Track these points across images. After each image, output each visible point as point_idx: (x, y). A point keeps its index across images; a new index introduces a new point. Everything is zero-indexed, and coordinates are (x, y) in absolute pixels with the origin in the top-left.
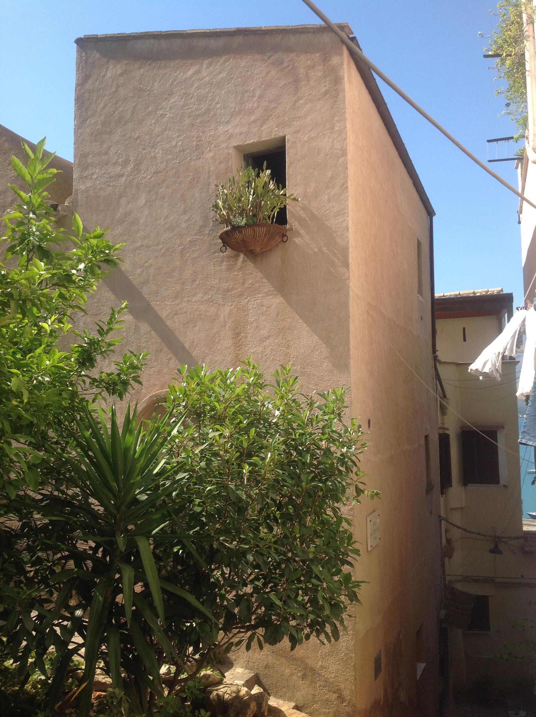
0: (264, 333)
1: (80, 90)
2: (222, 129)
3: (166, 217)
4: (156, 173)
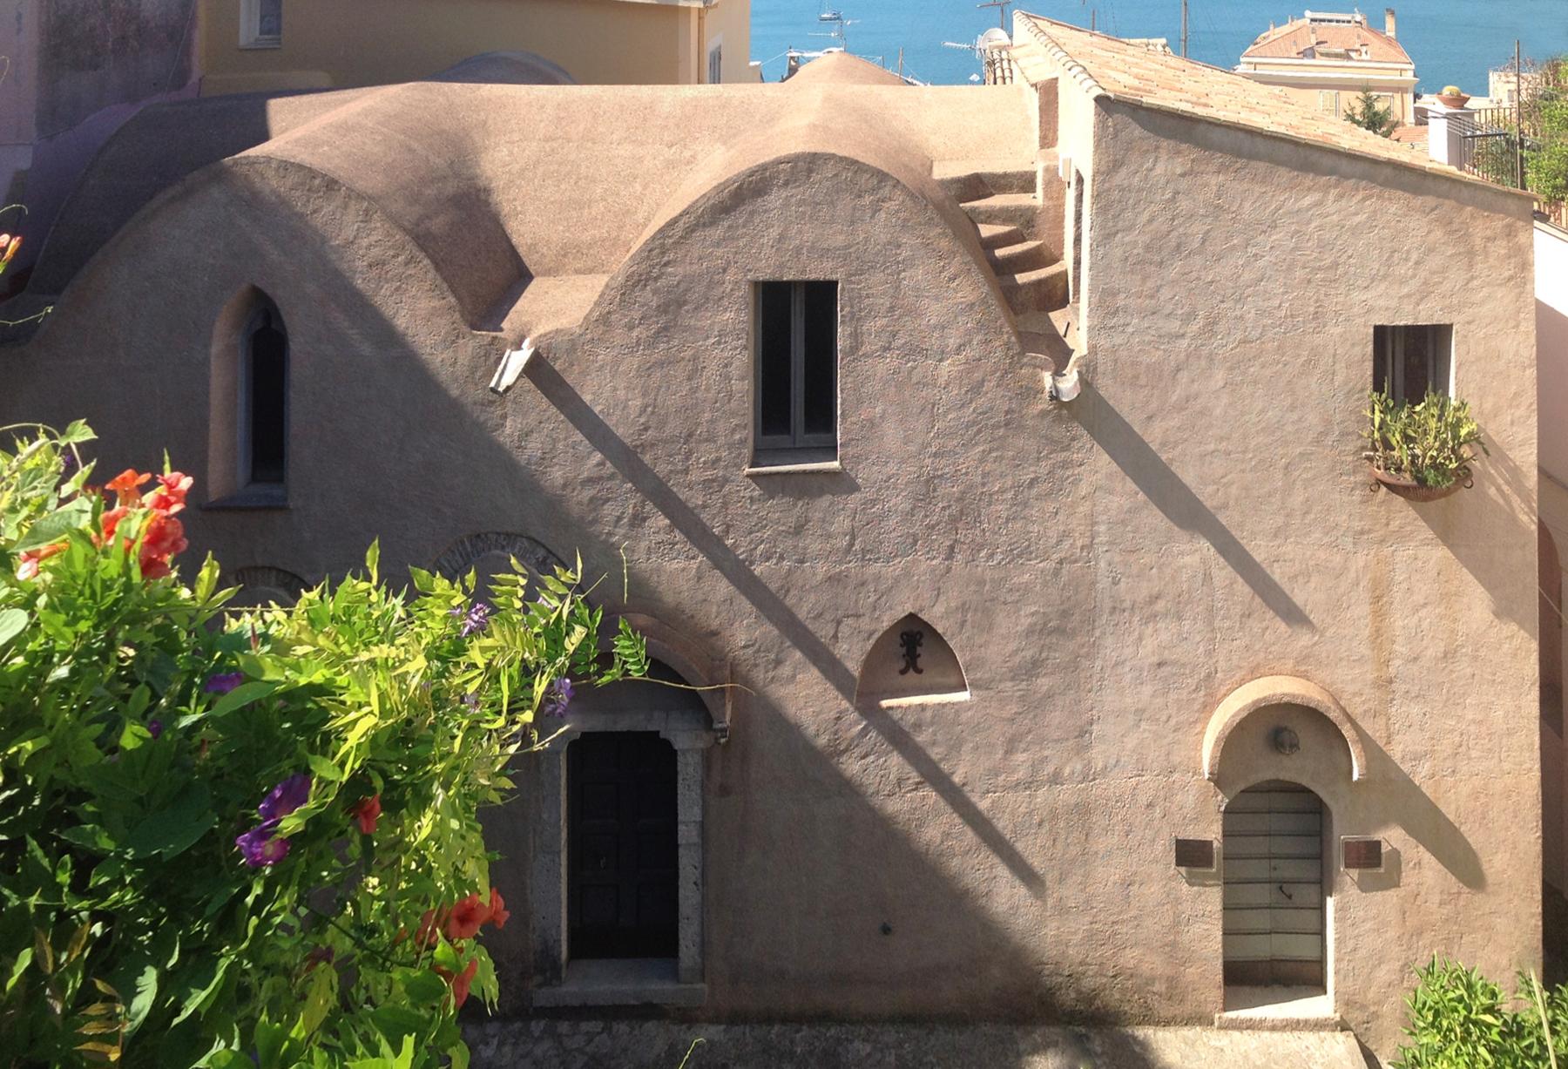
0: (1419, 598)
1: (1104, 181)
2: (1357, 296)
3: (1263, 411)
4: (1244, 341)
